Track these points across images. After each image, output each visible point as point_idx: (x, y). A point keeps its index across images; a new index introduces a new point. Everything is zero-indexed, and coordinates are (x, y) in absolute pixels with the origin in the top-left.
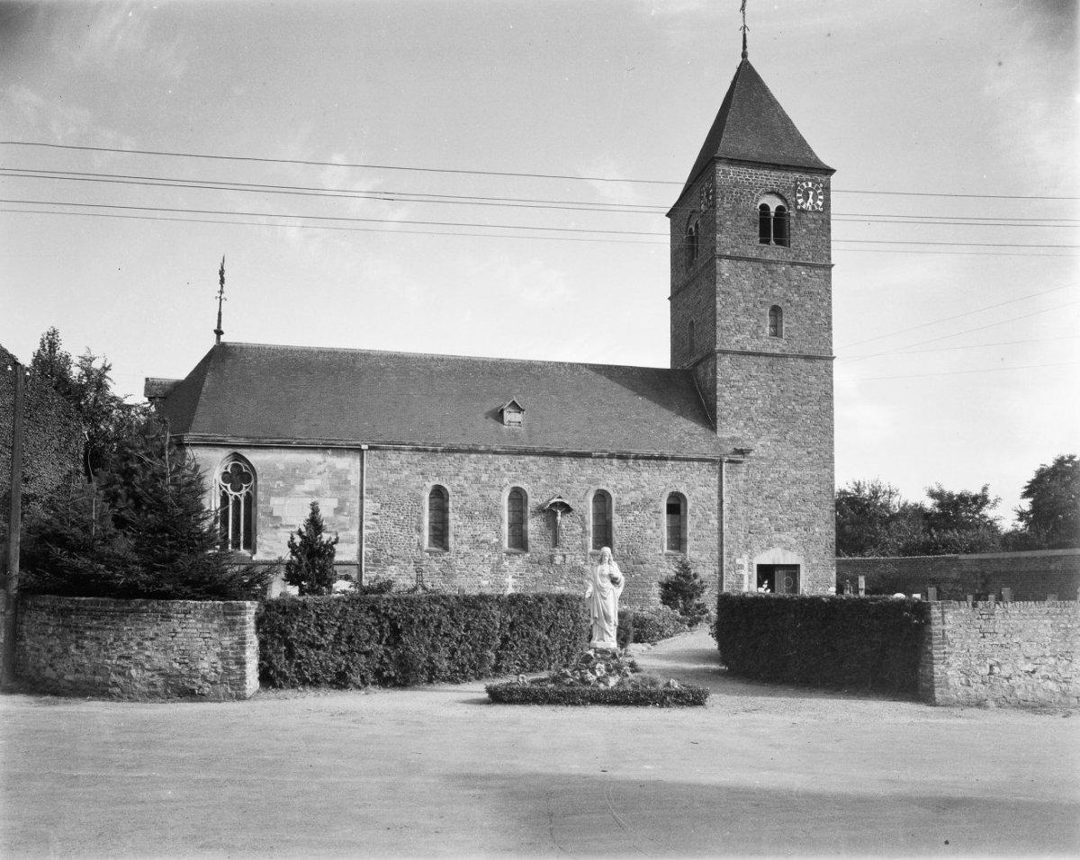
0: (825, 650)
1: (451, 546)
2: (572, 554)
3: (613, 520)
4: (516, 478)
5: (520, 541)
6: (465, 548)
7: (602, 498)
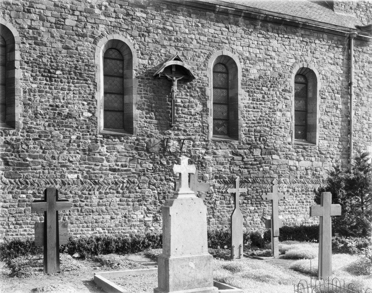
1: (19, 119)
2: (190, 139)
3: (240, 97)
4: (117, 27)
5: (120, 121)
6: (41, 125)
7: (226, 66)
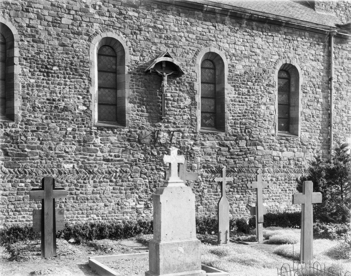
0: (202, 159)
1: (18, 112)
2: (179, 131)
3: (226, 92)
4: (111, 26)
5: (113, 114)
6: (39, 117)
7: (213, 62)
